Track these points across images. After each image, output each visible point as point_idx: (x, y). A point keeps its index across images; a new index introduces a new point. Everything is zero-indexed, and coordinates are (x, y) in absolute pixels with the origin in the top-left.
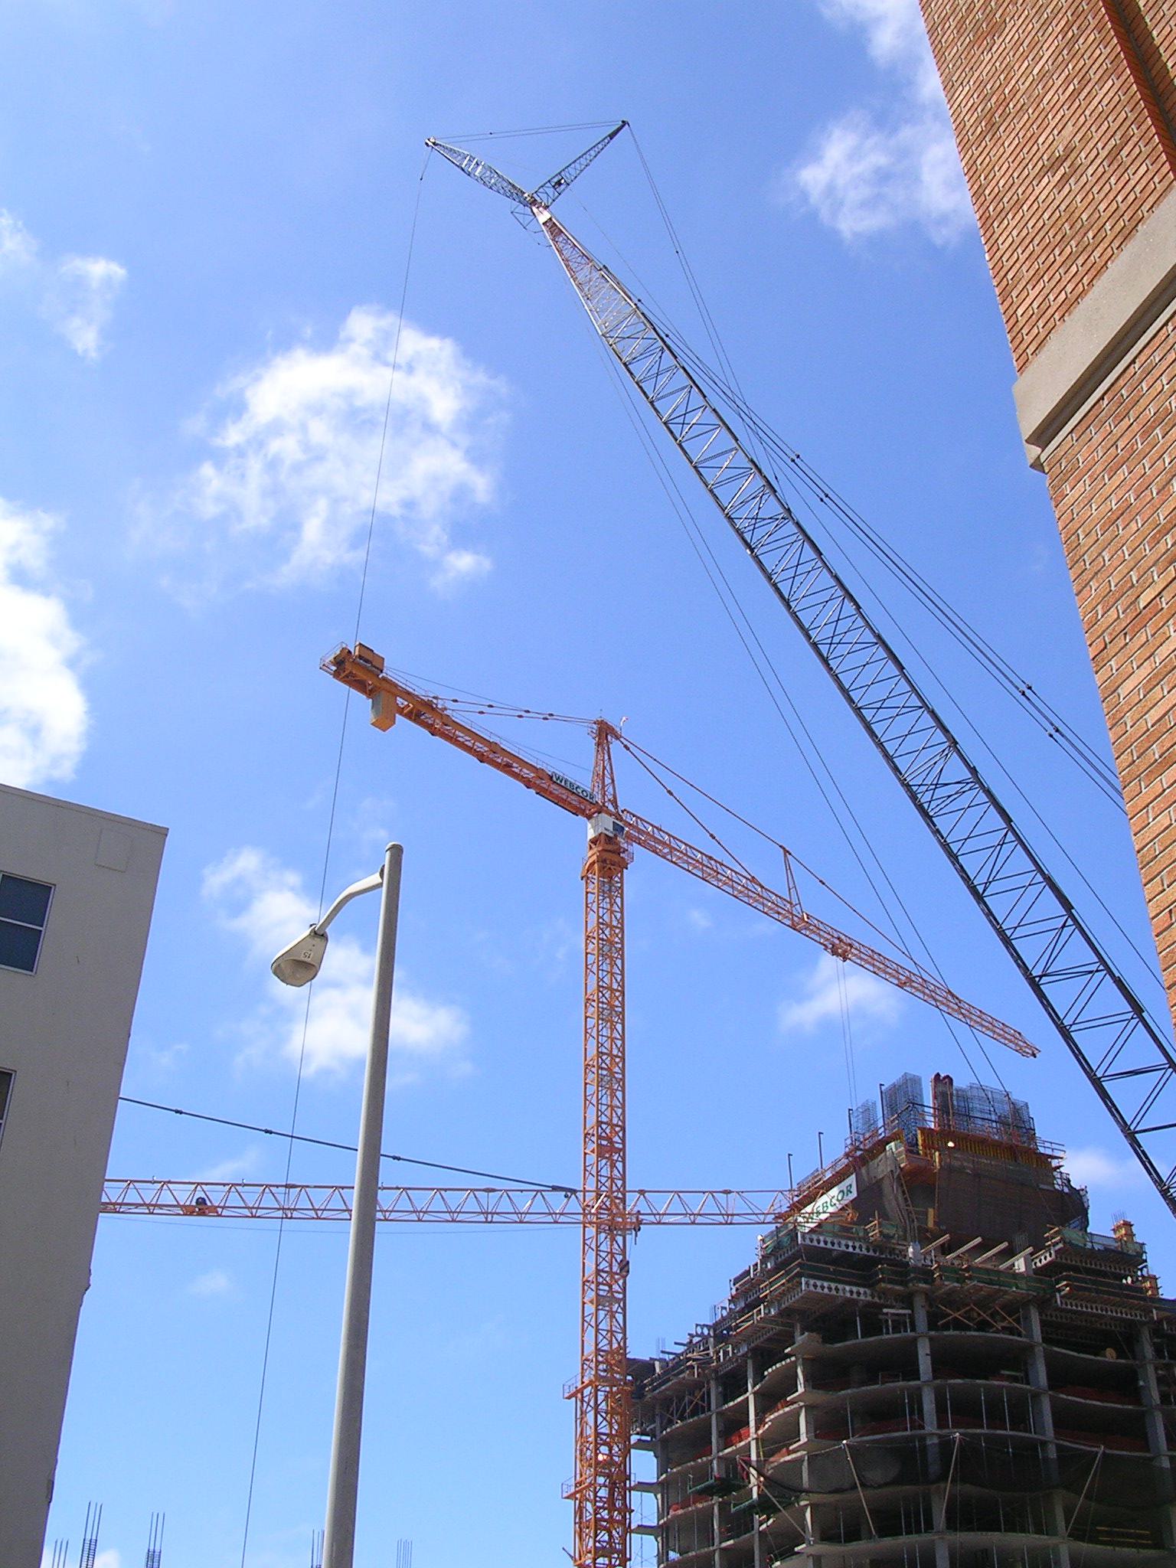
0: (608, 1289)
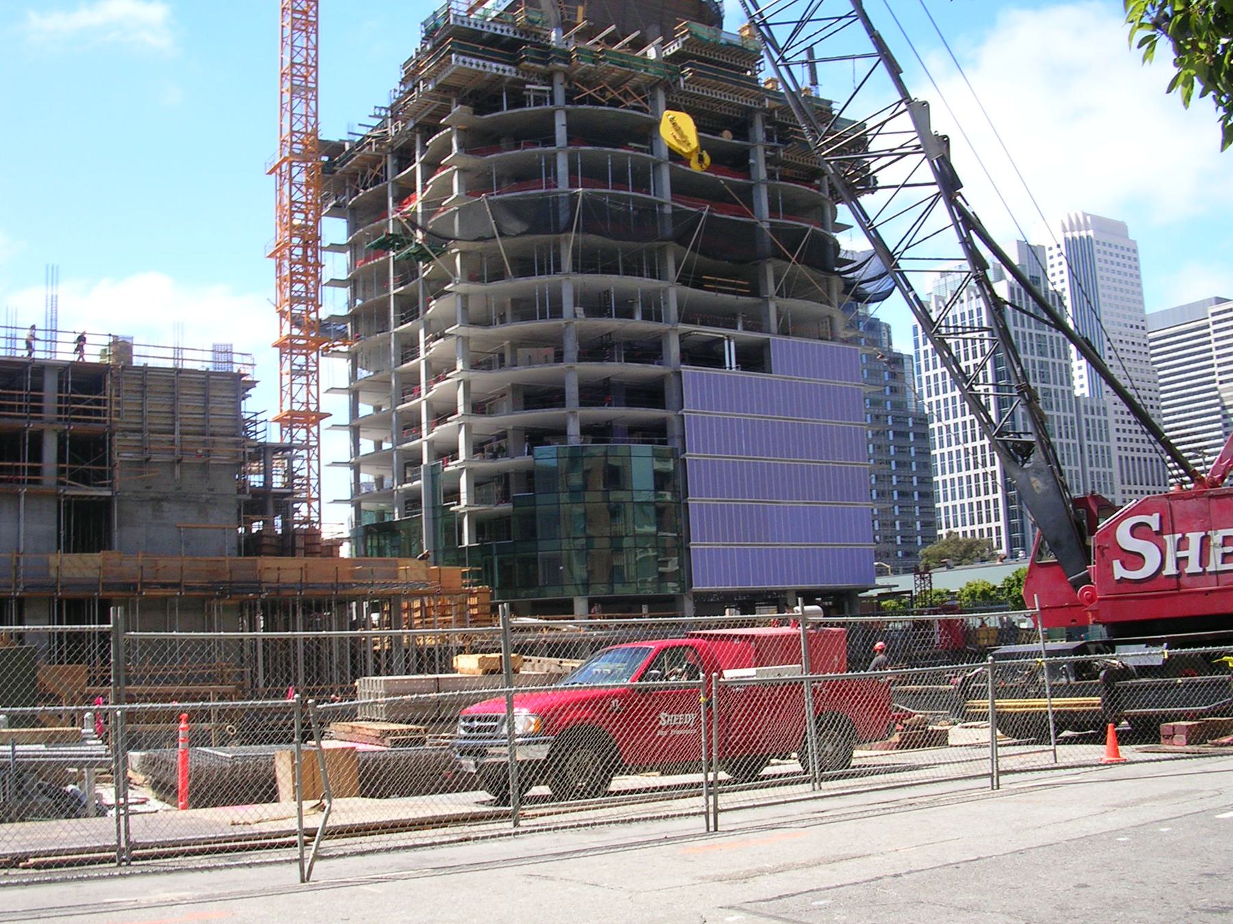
0: (302, 82)
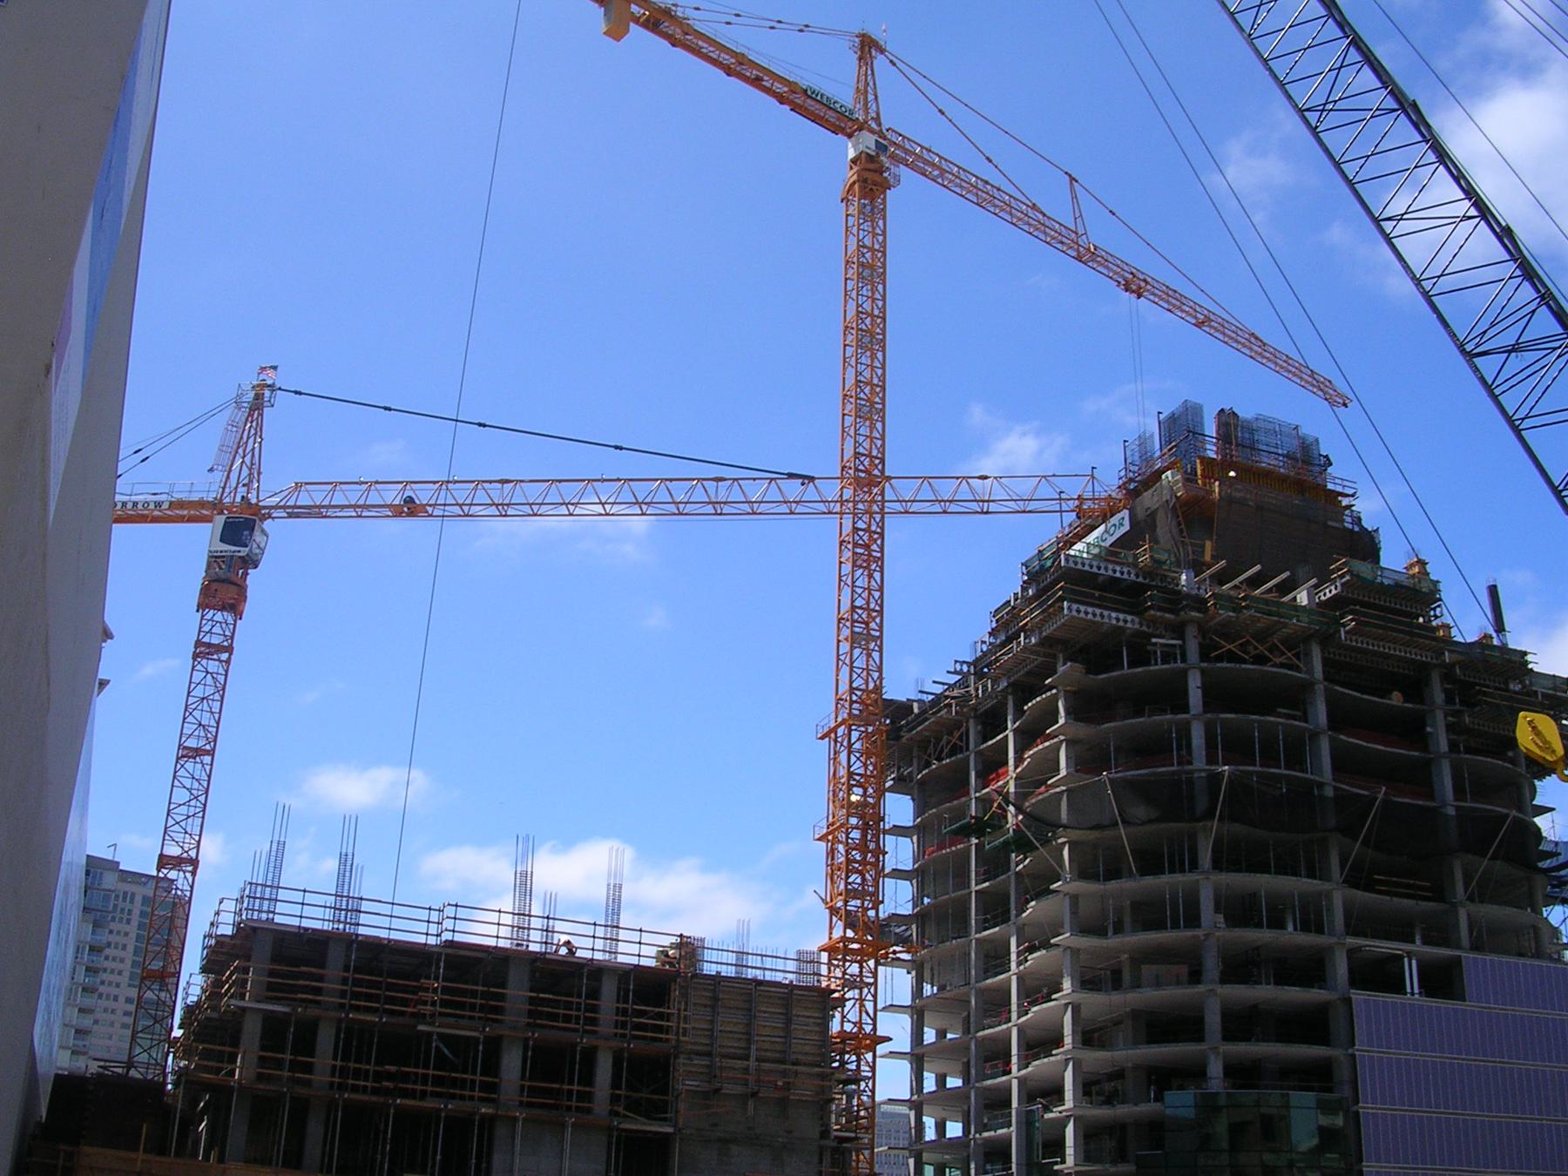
0: (863, 629)
